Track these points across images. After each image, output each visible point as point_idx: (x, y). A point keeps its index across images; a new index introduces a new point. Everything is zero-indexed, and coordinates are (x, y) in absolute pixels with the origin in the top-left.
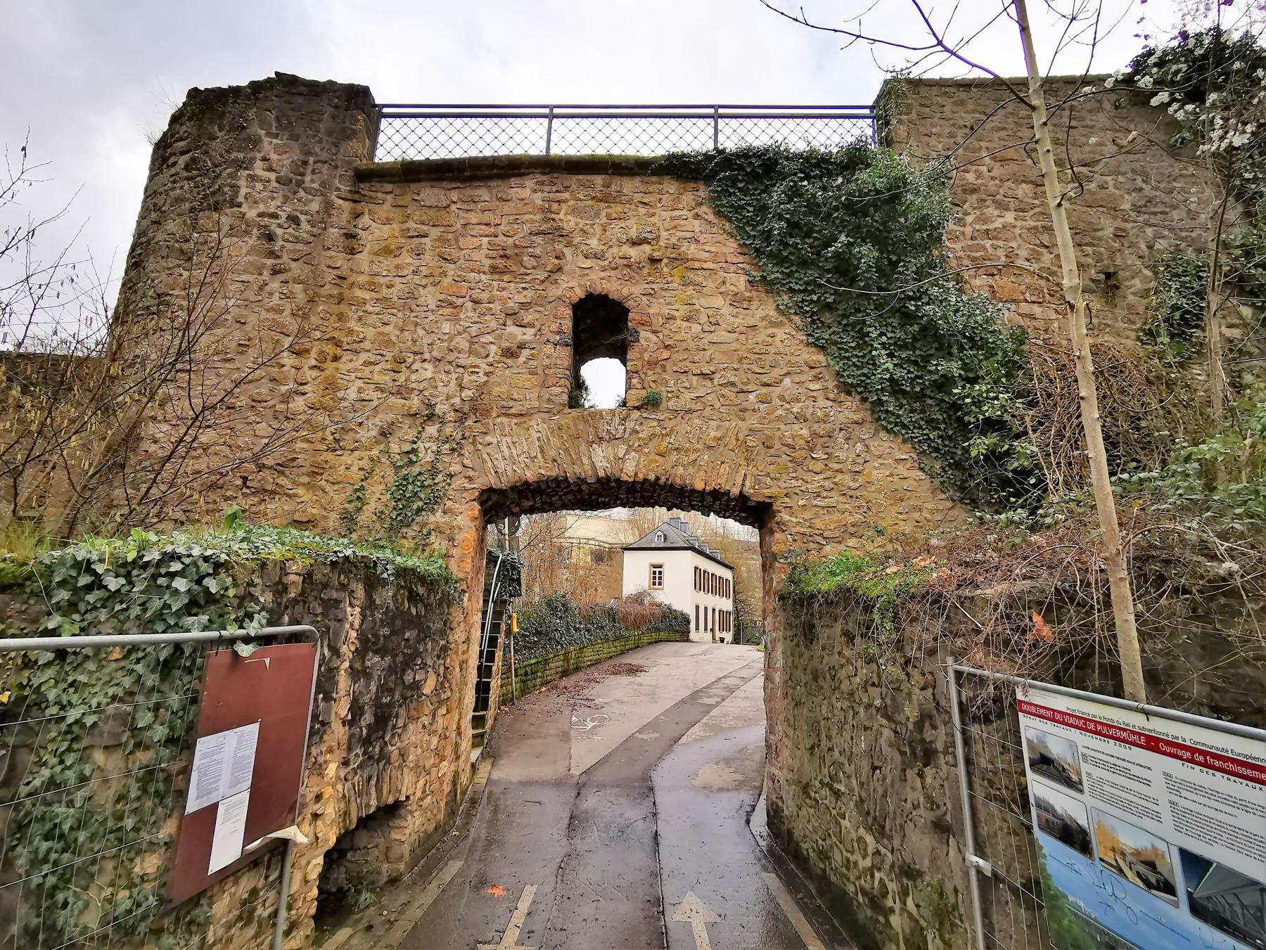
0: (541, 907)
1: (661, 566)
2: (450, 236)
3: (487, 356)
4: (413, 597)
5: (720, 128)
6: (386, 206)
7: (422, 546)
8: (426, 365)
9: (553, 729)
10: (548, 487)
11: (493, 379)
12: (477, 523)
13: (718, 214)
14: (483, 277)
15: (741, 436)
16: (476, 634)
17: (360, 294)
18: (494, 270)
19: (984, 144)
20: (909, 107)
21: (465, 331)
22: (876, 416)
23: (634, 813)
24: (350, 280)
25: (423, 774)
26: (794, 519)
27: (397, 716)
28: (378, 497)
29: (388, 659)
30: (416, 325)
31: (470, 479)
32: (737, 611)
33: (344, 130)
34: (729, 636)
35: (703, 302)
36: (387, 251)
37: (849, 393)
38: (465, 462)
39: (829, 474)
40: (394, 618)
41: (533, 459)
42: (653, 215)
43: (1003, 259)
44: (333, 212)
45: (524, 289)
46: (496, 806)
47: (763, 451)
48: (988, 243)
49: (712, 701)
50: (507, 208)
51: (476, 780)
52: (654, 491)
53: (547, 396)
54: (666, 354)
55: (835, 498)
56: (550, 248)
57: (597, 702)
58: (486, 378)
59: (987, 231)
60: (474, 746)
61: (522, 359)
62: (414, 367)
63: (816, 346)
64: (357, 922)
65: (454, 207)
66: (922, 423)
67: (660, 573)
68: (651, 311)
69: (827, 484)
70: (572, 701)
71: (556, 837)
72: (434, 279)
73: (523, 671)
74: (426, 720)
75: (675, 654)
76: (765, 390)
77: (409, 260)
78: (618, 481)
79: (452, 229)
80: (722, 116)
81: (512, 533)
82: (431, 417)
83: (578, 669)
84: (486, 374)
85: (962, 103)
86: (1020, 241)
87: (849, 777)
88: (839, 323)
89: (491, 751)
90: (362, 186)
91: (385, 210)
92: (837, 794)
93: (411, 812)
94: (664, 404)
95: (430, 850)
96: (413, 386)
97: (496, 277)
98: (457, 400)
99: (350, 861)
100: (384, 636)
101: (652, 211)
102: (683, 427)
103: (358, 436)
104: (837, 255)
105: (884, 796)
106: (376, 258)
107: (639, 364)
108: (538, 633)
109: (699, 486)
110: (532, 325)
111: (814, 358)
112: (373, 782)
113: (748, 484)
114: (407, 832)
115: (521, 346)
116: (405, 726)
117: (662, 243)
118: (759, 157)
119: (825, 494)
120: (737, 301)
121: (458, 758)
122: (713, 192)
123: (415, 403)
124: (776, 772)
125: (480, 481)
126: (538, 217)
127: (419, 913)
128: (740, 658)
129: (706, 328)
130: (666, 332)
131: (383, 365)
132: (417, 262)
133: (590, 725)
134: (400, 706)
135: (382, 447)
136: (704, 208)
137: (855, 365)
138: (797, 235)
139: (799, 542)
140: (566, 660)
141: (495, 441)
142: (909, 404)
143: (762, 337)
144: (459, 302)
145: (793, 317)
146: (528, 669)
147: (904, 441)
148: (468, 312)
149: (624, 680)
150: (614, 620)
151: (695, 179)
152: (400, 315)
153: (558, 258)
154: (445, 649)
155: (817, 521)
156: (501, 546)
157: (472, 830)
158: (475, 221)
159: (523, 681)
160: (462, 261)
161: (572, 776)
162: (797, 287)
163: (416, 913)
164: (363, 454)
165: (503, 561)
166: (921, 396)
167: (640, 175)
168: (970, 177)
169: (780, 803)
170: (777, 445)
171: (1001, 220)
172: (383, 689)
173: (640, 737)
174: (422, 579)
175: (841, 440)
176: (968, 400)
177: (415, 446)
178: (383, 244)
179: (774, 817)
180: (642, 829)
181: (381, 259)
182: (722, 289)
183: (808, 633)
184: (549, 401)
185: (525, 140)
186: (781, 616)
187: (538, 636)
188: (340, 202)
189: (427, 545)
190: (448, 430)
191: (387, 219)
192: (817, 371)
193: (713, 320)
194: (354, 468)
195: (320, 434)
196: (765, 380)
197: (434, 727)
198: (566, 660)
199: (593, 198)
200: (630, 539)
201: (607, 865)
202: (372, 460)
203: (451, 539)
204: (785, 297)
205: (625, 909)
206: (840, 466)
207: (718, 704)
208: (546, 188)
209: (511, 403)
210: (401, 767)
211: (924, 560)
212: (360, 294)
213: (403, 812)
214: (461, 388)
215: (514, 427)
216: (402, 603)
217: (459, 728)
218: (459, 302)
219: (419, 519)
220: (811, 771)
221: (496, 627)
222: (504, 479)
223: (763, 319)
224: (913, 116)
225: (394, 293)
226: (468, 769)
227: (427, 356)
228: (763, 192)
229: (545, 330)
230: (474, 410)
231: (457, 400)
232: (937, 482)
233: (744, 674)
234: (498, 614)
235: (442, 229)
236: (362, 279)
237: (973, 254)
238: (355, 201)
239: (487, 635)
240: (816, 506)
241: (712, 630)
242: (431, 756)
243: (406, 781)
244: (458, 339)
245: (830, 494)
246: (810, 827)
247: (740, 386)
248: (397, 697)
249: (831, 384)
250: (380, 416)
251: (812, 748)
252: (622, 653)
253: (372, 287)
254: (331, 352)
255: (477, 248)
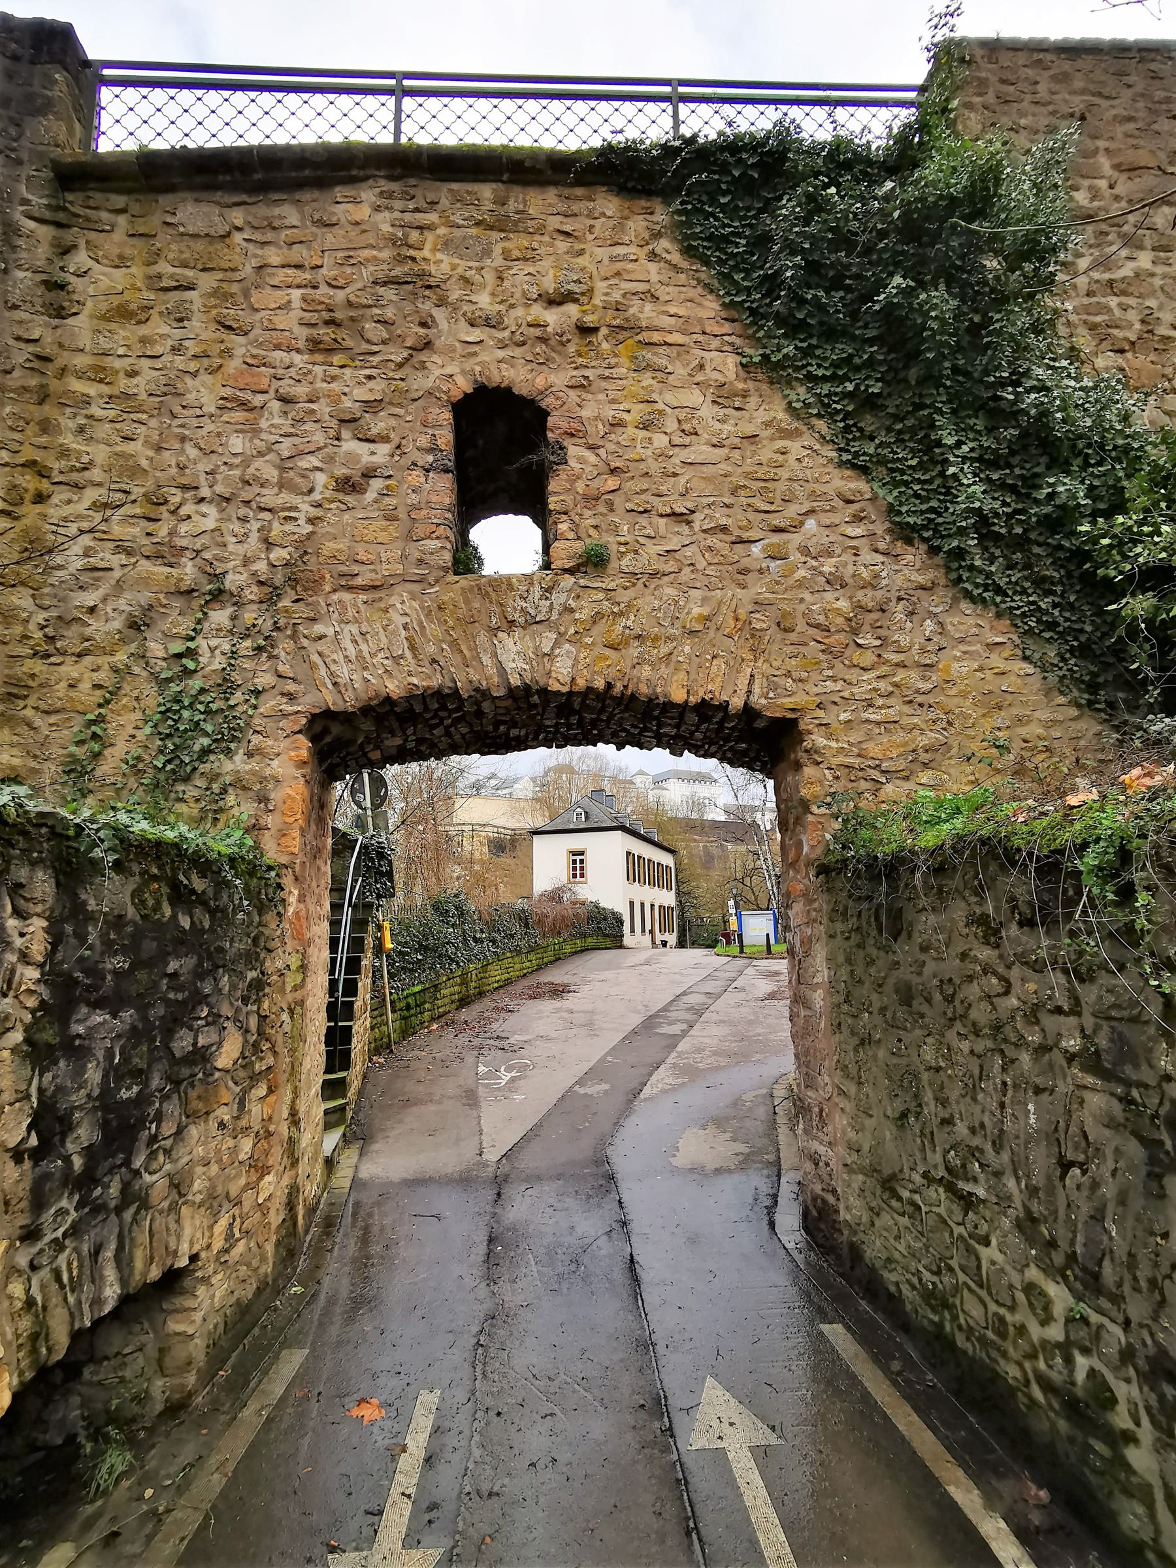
0: (451, 1440)
1: (582, 853)
2: (235, 288)
3: (311, 491)
4: (181, 896)
5: (682, 117)
6: (118, 236)
7: (214, 813)
8: (204, 508)
9: (450, 1087)
10: (426, 709)
11: (323, 528)
12: (307, 770)
13: (688, 251)
14: (297, 359)
15: (742, 613)
16: (321, 955)
17: (79, 386)
18: (315, 346)
19: (1101, 144)
20: (983, 84)
21: (270, 450)
22: (954, 576)
23: (590, 1224)
24: (59, 363)
25: (226, 1206)
26: (834, 744)
27: (159, 1117)
28: (129, 733)
29: (128, 1015)
30: (183, 439)
31: (291, 697)
32: (681, 904)
33: (30, 97)
34: (672, 939)
35: (669, 397)
36: (123, 314)
37: (909, 542)
38: (281, 668)
39: (884, 670)
40: (138, 936)
41: (397, 659)
42: (581, 253)
43: (1138, 326)
44: (21, 242)
45: (370, 378)
46: (366, 1230)
47: (779, 636)
48: (1113, 302)
49: (676, 1029)
50: (330, 238)
51: (335, 1182)
52: (602, 710)
53: (417, 555)
54: (612, 483)
55: (896, 709)
56: (408, 308)
57: (512, 1040)
58: (310, 528)
59: (1111, 283)
60: (328, 1126)
61: (370, 496)
62: (183, 511)
63: (854, 467)
64: (89, 1524)
65: (238, 237)
66: (1027, 584)
67: (582, 861)
68: (585, 413)
69: (882, 685)
70: (476, 1042)
71: (469, 1282)
72: (210, 361)
73: (403, 1004)
74: (224, 1114)
75: (610, 966)
76: (776, 538)
77: (165, 329)
78: (544, 692)
79: (238, 276)
80: (686, 99)
81: (376, 806)
82: (218, 596)
83: (481, 994)
84: (311, 521)
85: (1063, 78)
86: (1162, 298)
87: (998, 1174)
88: (889, 430)
89: (354, 1125)
90: (70, 197)
91: (116, 240)
92: (968, 1202)
93: (205, 1280)
94: (614, 564)
95: (249, 1335)
96: (183, 543)
97: (319, 358)
98: (261, 566)
99: (90, 1384)
100: (116, 973)
101: (578, 246)
102: (647, 602)
103: (88, 631)
104: (889, 306)
105: (1098, 1217)
106: (103, 325)
107: (569, 499)
108: (423, 949)
109: (678, 696)
110: (385, 439)
111: (852, 485)
112: (109, 1253)
113: (757, 690)
114: (198, 1316)
115: (369, 474)
116: (179, 1132)
117: (598, 301)
118: (754, 148)
119: (880, 702)
120: (723, 396)
121: (295, 1163)
122: (678, 212)
123: (188, 571)
124: (822, 1150)
125: (308, 699)
126: (385, 254)
127: (217, 1481)
128: (696, 966)
129: (677, 440)
130: (611, 447)
131: (128, 510)
132: (178, 334)
133: (506, 1077)
134: (166, 1098)
135: (132, 648)
136: (664, 244)
137: (916, 495)
138: (818, 286)
139: (843, 782)
140: (464, 983)
141: (330, 631)
142: (1005, 557)
143: (766, 453)
144: (258, 400)
145: (814, 421)
146: (411, 1000)
147: (999, 615)
148: (274, 418)
149: (547, 1006)
150: (527, 926)
151: (649, 193)
152: (153, 423)
153: (423, 325)
154: (258, 986)
155: (869, 745)
156: (360, 823)
157: (326, 1281)
158: (275, 260)
159: (404, 1018)
160: (257, 331)
161: (485, 1165)
162: (820, 372)
163: (211, 1483)
164: (100, 661)
165: (364, 847)
166: (1022, 543)
167: (555, 184)
168: (1081, 197)
169: (831, 1199)
170: (801, 626)
171: (1131, 265)
172: (116, 1074)
173: (582, 1091)
174: (202, 863)
175: (900, 616)
176: (1105, 542)
177: (191, 645)
178: (116, 301)
179: (818, 1220)
180: (607, 1251)
181: (113, 326)
182: (699, 378)
183: (895, 925)
184: (420, 562)
185: (363, 123)
186: (822, 902)
187: (422, 952)
188: (32, 224)
189: (221, 810)
190: (249, 615)
191: (121, 257)
192: (856, 506)
193: (687, 427)
194: (86, 686)
195: (18, 630)
196: (776, 522)
197: (243, 1123)
198: (464, 983)
199: (478, 224)
200: (540, 822)
201: (558, 1333)
202: (116, 671)
203: (263, 799)
204: (802, 390)
205: (603, 1429)
206: (901, 657)
207: (684, 1033)
208: (398, 204)
209: (356, 568)
210: (174, 1208)
211: (1149, 774)
212: (79, 386)
213: (187, 1282)
214: (269, 544)
215: (362, 607)
216: (157, 908)
217: (293, 1113)
218: (258, 400)
219: (204, 768)
220: (895, 1152)
221: (357, 944)
222: (349, 695)
223: (767, 424)
224: (990, 98)
225: (139, 386)
226: (319, 1169)
227: (205, 492)
228: (761, 211)
229: (409, 448)
230: (293, 581)
231: (261, 566)
232: (1053, 678)
233: (710, 987)
234: (359, 924)
235: (220, 275)
236: (81, 361)
237: (1091, 318)
238: (59, 225)
239: (343, 955)
240: (867, 721)
241: (651, 932)
242: (222, 1189)
243: (187, 1231)
244: (258, 463)
245: (888, 702)
246: (901, 1248)
247: (737, 532)
248: (156, 1082)
249: (880, 528)
250: (127, 595)
251: (904, 1115)
252: (540, 968)
253: (100, 375)
254: (31, 487)
255: (285, 309)
